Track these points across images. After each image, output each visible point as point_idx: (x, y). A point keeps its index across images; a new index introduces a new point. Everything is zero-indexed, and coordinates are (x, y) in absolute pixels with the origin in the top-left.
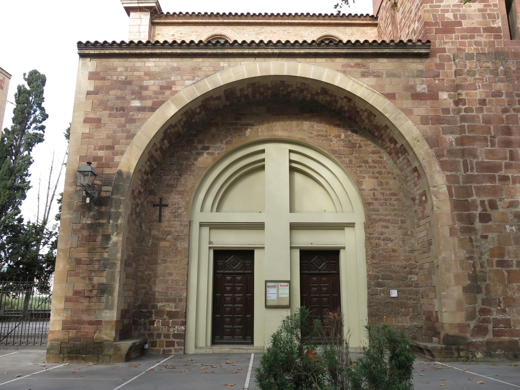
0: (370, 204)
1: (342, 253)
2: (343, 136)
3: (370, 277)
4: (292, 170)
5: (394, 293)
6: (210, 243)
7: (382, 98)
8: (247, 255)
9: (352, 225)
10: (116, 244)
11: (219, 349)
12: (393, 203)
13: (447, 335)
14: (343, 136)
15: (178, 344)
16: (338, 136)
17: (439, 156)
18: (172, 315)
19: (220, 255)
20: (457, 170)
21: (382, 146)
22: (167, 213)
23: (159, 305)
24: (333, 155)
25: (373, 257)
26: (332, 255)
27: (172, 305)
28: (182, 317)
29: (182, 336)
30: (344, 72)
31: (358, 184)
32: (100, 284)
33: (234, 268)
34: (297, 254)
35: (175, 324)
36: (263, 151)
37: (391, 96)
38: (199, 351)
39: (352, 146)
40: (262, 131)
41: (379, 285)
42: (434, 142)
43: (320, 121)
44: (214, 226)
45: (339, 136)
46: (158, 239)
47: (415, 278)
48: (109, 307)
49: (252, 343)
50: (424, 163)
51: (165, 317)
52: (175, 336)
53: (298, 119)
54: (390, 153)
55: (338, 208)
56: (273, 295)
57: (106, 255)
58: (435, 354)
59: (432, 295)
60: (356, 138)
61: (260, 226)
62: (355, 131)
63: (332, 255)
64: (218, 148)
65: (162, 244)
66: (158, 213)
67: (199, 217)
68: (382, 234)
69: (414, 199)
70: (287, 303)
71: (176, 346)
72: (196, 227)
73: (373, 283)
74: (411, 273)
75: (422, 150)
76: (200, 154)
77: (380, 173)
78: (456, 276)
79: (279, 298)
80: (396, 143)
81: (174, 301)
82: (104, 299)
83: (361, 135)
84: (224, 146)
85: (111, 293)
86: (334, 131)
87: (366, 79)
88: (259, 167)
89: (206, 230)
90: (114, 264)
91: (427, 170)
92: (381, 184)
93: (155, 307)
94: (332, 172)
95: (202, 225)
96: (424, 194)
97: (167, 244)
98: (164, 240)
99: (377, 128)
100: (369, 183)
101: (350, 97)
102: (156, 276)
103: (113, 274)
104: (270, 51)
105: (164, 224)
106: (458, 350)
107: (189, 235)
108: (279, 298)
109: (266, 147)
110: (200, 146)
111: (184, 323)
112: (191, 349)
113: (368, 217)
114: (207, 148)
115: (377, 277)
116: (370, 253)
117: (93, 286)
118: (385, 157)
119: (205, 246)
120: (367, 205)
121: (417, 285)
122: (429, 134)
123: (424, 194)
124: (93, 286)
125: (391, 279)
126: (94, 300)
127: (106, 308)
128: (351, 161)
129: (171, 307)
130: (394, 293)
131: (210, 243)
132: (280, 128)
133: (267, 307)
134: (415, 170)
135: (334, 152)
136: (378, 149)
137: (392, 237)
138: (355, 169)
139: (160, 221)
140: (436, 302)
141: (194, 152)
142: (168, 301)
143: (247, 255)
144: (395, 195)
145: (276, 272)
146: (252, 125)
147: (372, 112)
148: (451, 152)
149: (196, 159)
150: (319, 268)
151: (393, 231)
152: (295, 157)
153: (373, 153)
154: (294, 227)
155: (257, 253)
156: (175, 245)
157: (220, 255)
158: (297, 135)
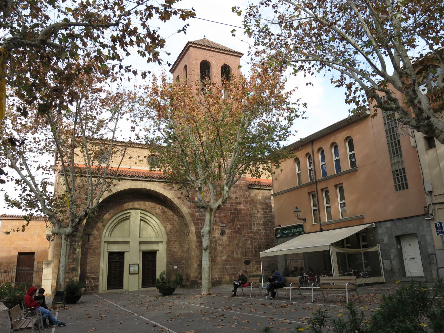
0: (169, 235)
1: (158, 253)
2: (161, 208)
3: (167, 262)
4: (141, 220)
5: (176, 267)
6: (108, 249)
7: (176, 199)
8: (121, 254)
9: (162, 242)
10: (78, 252)
11: (110, 291)
12: (177, 234)
13: (192, 280)
14: (161, 208)
15: (96, 289)
16: (159, 208)
17: (193, 220)
18: (93, 278)
19: (111, 254)
20: (199, 225)
21: (174, 213)
22: (91, 238)
23: (88, 275)
24: (157, 215)
25: (169, 254)
26: (154, 254)
27: (93, 274)
28: (96, 279)
29: (97, 286)
30: (164, 188)
31: (165, 227)
32: (72, 268)
33: (116, 259)
34: (141, 253)
35: (94, 282)
36: (130, 213)
37: (179, 198)
38: (103, 292)
39: (164, 212)
40: (130, 205)
41: (171, 264)
42: (192, 215)
43: (152, 202)
44: (109, 243)
45: (159, 208)
46: (87, 248)
47: (183, 261)
48: (76, 276)
49: (122, 287)
50: (188, 223)
51: (91, 279)
52: (95, 286)
53: (144, 201)
54: (177, 216)
55: (157, 235)
56: (132, 270)
57: (75, 256)
58: (188, 286)
59: (188, 268)
60: (165, 209)
61: (128, 243)
62: (165, 206)
63: (154, 254)
64: (112, 212)
65: (89, 250)
66: (87, 238)
67: (104, 239)
68: (173, 246)
69: (184, 233)
70: (137, 272)
71: (95, 291)
72: (102, 243)
73: (168, 264)
74: (182, 260)
75: (188, 218)
76: (105, 214)
77: (173, 223)
78: (196, 261)
79: (134, 270)
80: (180, 213)
81: (94, 273)
82: (74, 273)
83: (167, 208)
84: (115, 211)
85: (77, 271)
86: (158, 206)
87: (172, 191)
88: (128, 218)
89: (106, 244)
90: (78, 260)
91: (189, 225)
92: (173, 227)
93: (86, 276)
94: (154, 221)
95: (105, 242)
96: (188, 232)
97: (92, 250)
98: (90, 249)
99: (173, 207)
100: (169, 226)
101: (165, 197)
102: (87, 263)
103: (78, 263)
104: (138, 179)
105: (90, 242)
106: (195, 285)
107: (100, 247)
108: (134, 270)
109: (131, 211)
110: (105, 211)
111: (98, 282)
112: (100, 292)
113: (168, 239)
114: (108, 211)
115: (170, 262)
116: (168, 253)
117: (70, 268)
118: (176, 217)
119: (106, 251)
120: (168, 234)
121: (184, 264)
122: (191, 212)
123: (188, 232)
124: (70, 268)
125: (175, 262)
126: (70, 273)
127: (75, 276)
128: (163, 218)
129: (93, 276)
130: (176, 267)
131: (108, 249)
132: (136, 204)
133: (130, 274)
134: (185, 224)
135: (157, 214)
136: (173, 214)
137: (176, 247)
138: (165, 220)
139: (88, 241)
140: (189, 270)
141: (103, 213)
142: (92, 273)
143: (121, 254)
144: (178, 231)
145: (133, 259)
146: (126, 202)
147: (172, 203)
148: (197, 219)
149: (104, 216)
150: (149, 258)
151: (177, 245)
152: (142, 215)
153: (171, 215)
154: (141, 243)
155: (126, 254)
156: (95, 251)
157: (111, 254)
158: (143, 207)
